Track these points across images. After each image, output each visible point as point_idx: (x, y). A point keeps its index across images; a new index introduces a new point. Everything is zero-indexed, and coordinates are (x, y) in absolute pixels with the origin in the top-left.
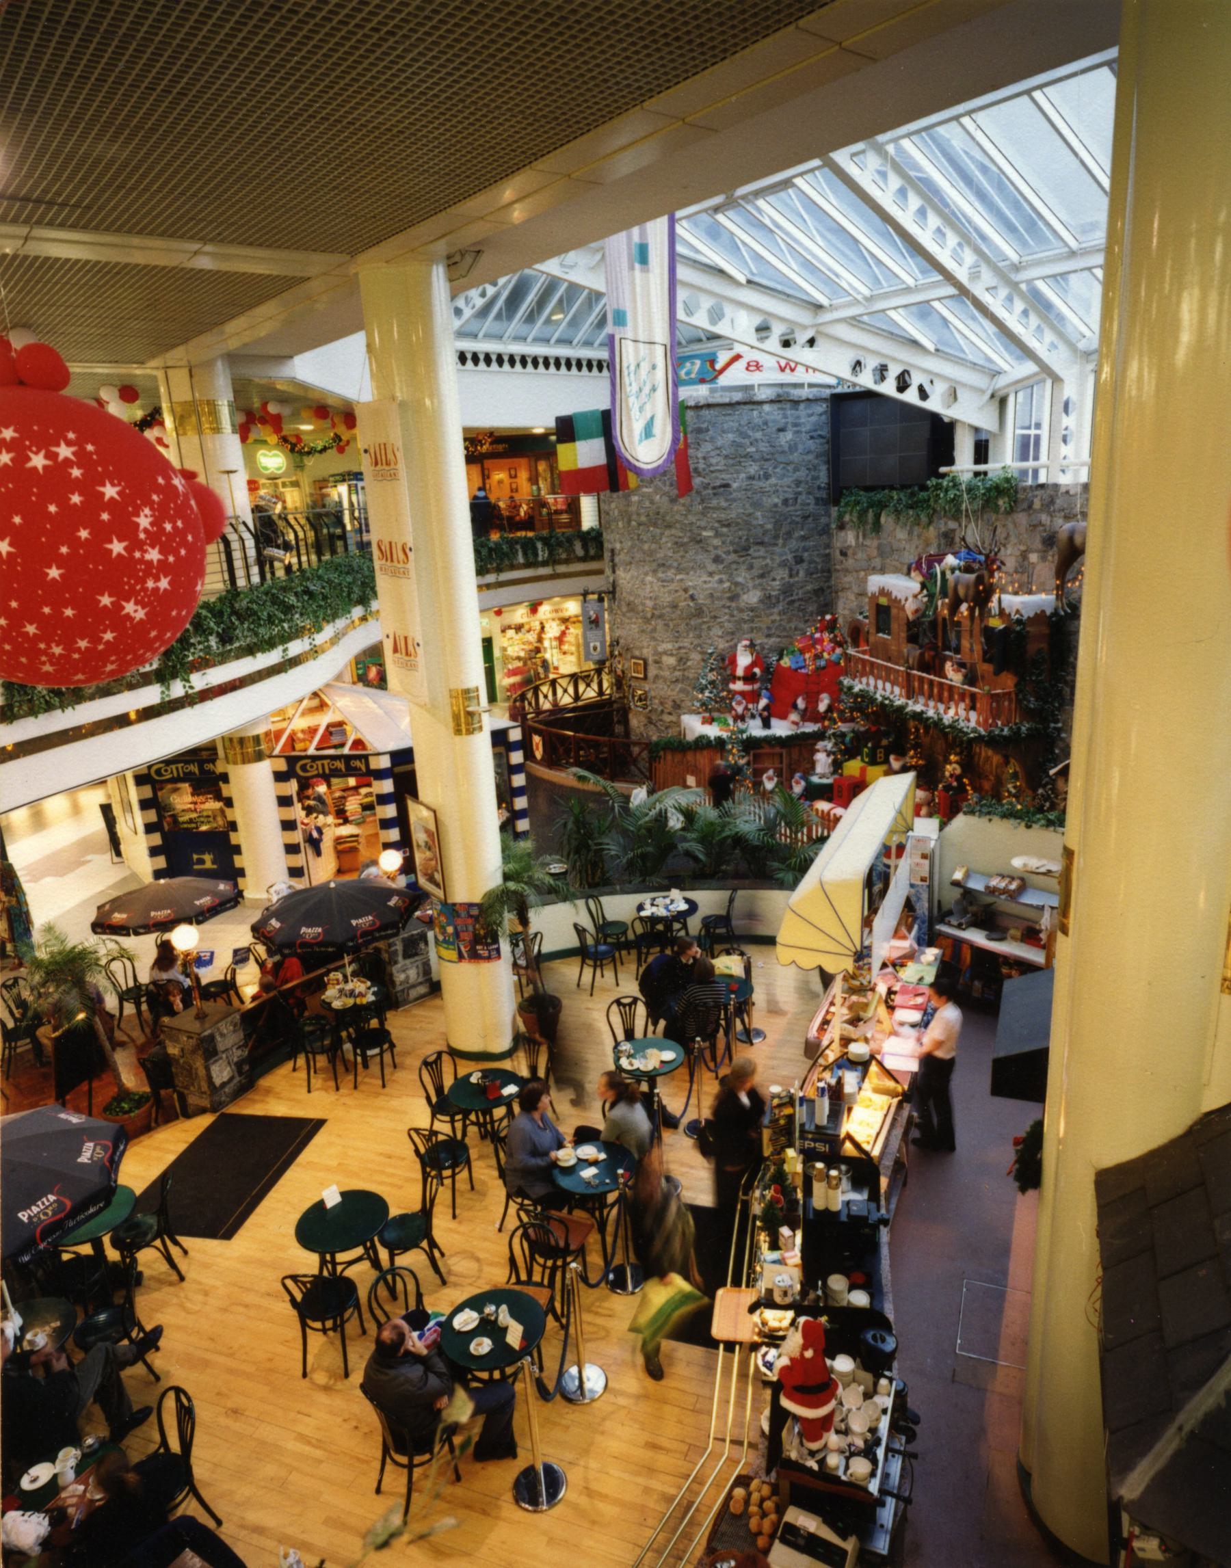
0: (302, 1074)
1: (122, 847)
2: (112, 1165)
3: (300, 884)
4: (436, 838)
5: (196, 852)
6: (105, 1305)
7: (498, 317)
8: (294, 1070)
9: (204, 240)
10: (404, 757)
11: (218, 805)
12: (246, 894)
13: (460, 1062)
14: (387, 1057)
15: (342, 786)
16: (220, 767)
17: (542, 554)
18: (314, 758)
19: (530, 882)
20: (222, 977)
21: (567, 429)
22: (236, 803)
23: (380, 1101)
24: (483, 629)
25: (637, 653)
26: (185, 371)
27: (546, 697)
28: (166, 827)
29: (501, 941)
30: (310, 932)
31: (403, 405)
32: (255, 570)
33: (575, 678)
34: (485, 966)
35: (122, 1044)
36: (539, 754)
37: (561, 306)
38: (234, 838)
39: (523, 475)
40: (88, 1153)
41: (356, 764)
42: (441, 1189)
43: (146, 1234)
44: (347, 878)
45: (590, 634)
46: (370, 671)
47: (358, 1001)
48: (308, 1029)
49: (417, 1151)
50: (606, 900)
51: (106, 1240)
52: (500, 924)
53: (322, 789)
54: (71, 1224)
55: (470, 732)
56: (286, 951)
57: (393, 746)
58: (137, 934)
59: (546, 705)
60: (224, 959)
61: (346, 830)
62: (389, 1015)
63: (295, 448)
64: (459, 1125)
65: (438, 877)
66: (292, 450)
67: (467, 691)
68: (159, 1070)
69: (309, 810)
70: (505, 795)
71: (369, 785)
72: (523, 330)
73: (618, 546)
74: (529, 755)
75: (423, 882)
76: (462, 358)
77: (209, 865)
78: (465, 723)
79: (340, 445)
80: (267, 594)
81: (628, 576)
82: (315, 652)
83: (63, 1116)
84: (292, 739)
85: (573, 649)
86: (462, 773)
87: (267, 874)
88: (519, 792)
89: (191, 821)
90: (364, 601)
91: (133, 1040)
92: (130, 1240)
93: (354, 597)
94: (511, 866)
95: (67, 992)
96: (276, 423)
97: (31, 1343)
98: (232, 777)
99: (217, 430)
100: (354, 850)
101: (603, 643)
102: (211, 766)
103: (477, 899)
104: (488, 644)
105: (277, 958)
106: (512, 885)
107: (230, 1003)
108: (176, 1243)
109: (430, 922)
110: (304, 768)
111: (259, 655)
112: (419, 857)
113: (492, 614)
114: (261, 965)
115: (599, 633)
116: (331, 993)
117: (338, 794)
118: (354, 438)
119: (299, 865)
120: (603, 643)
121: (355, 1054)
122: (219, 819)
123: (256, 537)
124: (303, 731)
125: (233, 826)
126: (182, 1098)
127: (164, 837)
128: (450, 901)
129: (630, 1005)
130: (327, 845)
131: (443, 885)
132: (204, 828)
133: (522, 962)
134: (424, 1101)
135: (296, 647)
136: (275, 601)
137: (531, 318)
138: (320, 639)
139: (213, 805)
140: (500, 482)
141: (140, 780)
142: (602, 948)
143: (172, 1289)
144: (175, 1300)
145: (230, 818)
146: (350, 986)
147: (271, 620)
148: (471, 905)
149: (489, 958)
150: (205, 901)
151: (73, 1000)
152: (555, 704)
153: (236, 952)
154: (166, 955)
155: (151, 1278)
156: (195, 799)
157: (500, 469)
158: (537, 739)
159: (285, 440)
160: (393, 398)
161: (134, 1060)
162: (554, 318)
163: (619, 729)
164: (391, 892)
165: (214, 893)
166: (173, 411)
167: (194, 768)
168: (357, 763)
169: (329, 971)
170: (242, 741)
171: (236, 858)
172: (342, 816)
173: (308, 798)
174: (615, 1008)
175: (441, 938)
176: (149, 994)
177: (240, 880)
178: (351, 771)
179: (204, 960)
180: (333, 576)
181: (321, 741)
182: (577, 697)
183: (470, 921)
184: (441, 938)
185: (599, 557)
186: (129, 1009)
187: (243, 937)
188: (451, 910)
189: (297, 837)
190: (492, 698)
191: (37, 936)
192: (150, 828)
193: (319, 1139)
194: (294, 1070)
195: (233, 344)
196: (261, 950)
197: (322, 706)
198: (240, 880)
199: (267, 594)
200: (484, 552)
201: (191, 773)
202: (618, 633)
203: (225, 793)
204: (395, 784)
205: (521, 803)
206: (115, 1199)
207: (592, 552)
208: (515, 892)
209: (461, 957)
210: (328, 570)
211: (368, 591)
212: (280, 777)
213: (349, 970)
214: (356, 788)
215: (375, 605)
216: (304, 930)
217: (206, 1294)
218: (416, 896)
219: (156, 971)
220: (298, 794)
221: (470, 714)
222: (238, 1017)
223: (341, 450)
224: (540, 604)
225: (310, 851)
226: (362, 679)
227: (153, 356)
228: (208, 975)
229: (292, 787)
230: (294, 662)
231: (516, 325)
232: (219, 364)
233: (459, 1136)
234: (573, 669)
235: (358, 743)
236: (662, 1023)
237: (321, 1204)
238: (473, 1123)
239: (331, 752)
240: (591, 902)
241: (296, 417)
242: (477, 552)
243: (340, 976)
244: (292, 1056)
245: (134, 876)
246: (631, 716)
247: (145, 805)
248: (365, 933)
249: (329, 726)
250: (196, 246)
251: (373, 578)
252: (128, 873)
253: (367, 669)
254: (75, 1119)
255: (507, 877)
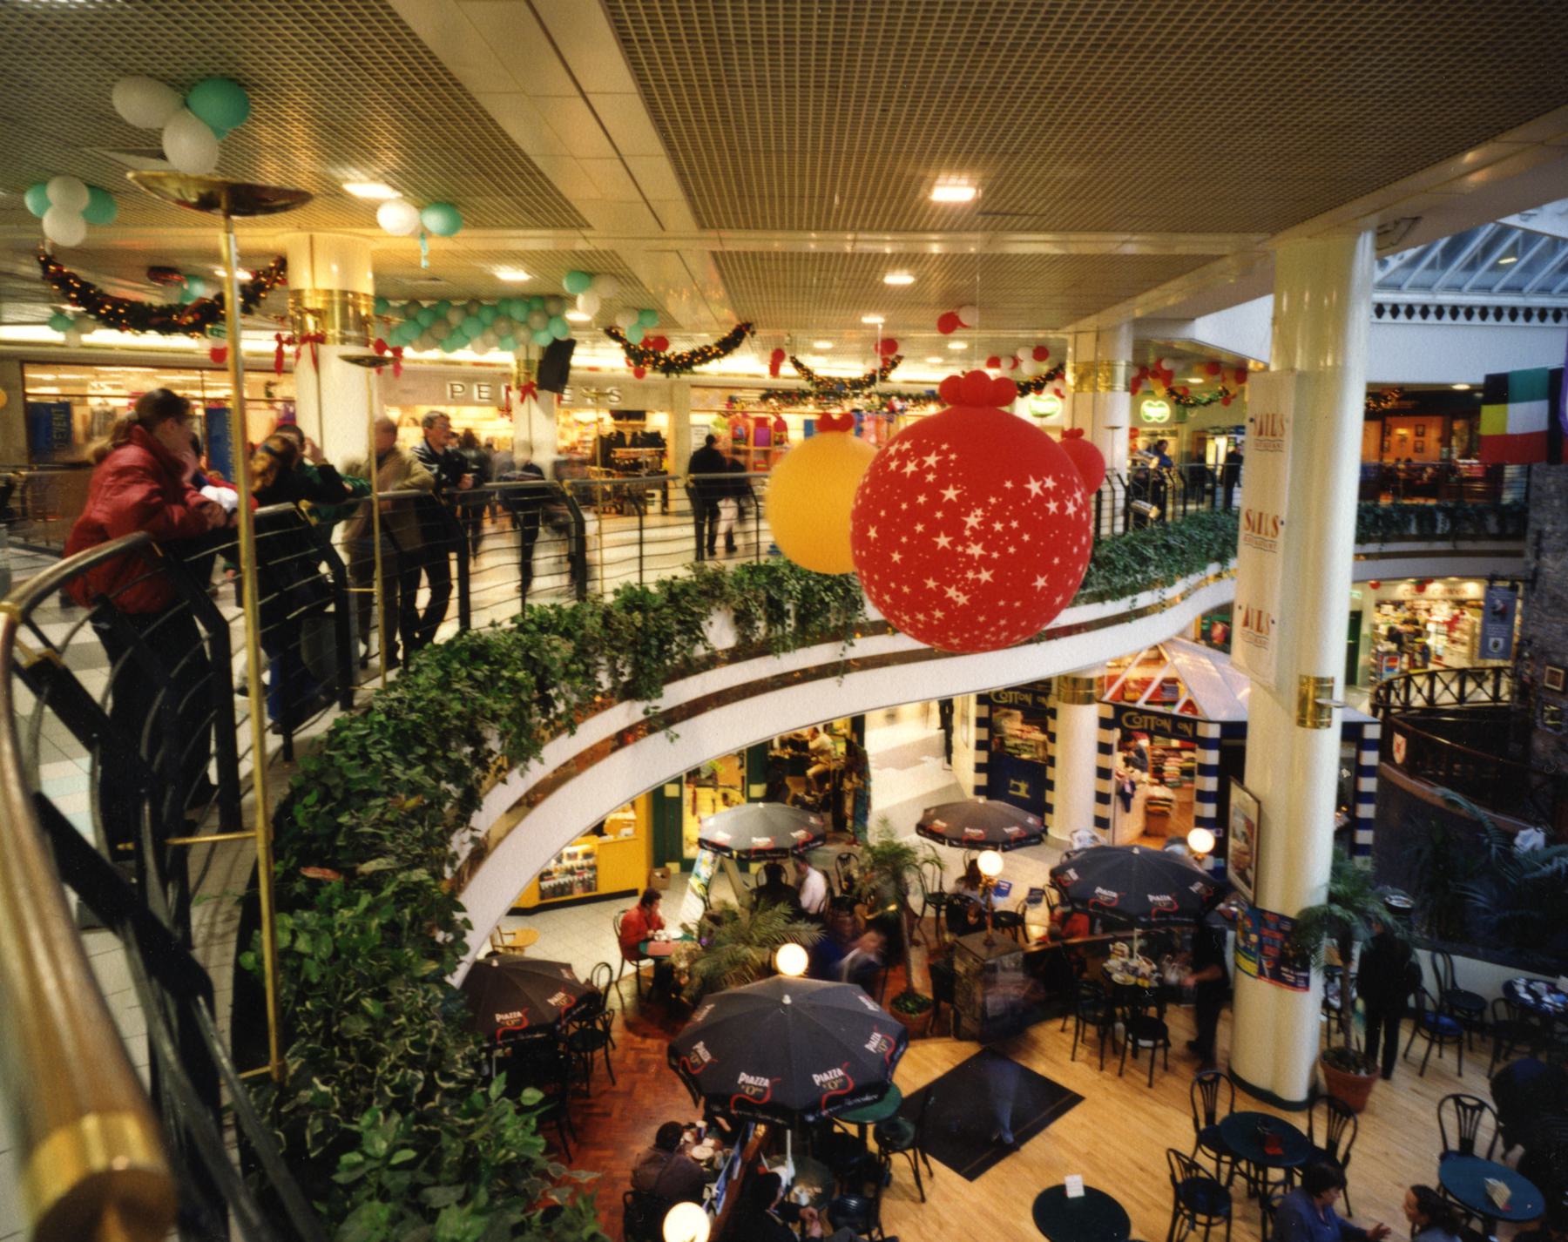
0: (1070, 1038)
1: (954, 756)
2: (891, 1062)
3: (1104, 839)
4: (1256, 831)
5: (1015, 780)
6: (857, 1193)
7: (1432, 266)
8: (1063, 1030)
9: (1134, 232)
10: (1235, 732)
11: (1042, 737)
12: (1050, 831)
13: (1240, 1093)
14: (1160, 1054)
15: (1164, 745)
16: (1051, 702)
17: (1442, 525)
18: (1142, 712)
19: (1361, 913)
20: (1013, 910)
21: (1498, 388)
22: (1058, 739)
23: (1144, 1101)
24: (1353, 601)
25: (1557, 659)
26: (1092, 336)
27: (1419, 691)
28: (994, 747)
29: (1313, 971)
30: (1105, 894)
31: (1302, 376)
32: (1120, 520)
33: (1462, 675)
34: (1289, 993)
35: (917, 944)
36: (1399, 756)
37: (1512, 251)
38: (1051, 773)
39: (1433, 434)
40: (875, 1043)
41: (1184, 728)
42: (1192, 1233)
43: (902, 1139)
44: (1153, 845)
45: (1492, 627)
46: (1215, 631)
47: (1140, 982)
48: (1084, 992)
49: (1173, 1177)
50: (1458, 960)
51: (870, 1129)
52: (1314, 951)
53: (1144, 743)
54: (850, 1103)
55: (1317, 726)
56: (1078, 907)
57: (1224, 716)
58: (951, 845)
59: (1418, 701)
60: (1019, 893)
61: (1160, 792)
62: (1170, 1008)
63: (1181, 399)
64: (1225, 1168)
65: (1250, 874)
66: (1177, 402)
67: (1320, 681)
68: (942, 977)
69: (1128, 761)
70: (1348, 797)
71: (1193, 750)
72: (1460, 278)
73: (1548, 528)
74: (1386, 755)
75: (1232, 874)
76: (1380, 310)
77: (1022, 793)
78: (1311, 712)
79: (1226, 398)
80: (1126, 544)
81: (1558, 566)
82: (1162, 606)
83: (862, 999)
84: (1123, 688)
85: (1466, 638)
86: (1300, 769)
87: (1074, 819)
88: (1367, 798)
89: (1016, 747)
90: (1222, 558)
91: (927, 943)
92: (891, 1140)
93: (1213, 554)
94: (1340, 887)
95: (886, 883)
96: (1167, 377)
97: (797, 1196)
98: (1060, 715)
99: (1111, 388)
100: (1164, 815)
101: (1508, 641)
102: (1043, 700)
103: (1292, 913)
104: (1356, 618)
105: (1068, 909)
106: (1337, 909)
107: (1015, 939)
108: (925, 1161)
109: (1232, 921)
110: (1129, 720)
111: (1109, 603)
112: (1233, 844)
113: (1367, 586)
114: (1052, 908)
115: (1505, 627)
116: (1113, 963)
117: (1158, 752)
118: (1242, 391)
119: (1106, 815)
120: (1508, 641)
121: (1127, 1039)
122: (1041, 750)
123: (1127, 489)
124: (1136, 682)
125: (1051, 761)
126: (957, 1017)
127: (990, 757)
128: (1259, 906)
129: (1473, 1109)
130: (1138, 802)
131: (1256, 885)
132: (1025, 756)
133: (1336, 1003)
134: (1190, 1122)
135: (1144, 599)
136: (1134, 552)
137: (1472, 266)
138: (1171, 593)
139: (1038, 736)
140: (1403, 439)
141: (983, 699)
142: (1446, 1020)
143: (912, 1205)
144: (913, 1219)
145: (1050, 753)
146: (1134, 963)
147: (1126, 570)
148: (1282, 918)
149: (1294, 985)
150: (1013, 830)
151: (889, 890)
152: (1431, 700)
153: (1032, 890)
154: (972, 874)
155: (899, 1185)
156: (1026, 728)
157: (1402, 427)
158: (1399, 740)
159: (1171, 392)
160: (1292, 370)
161: (925, 964)
162: (1504, 262)
163: (1514, 748)
164: (1194, 876)
165: (1024, 825)
166: (1075, 370)
167: (1028, 698)
168: (1185, 727)
169: (1113, 941)
170: (1075, 681)
171: (1048, 793)
172: (1159, 775)
173: (1128, 749)
174: (1451, 1103)
175: (1242, 944)
176: (949, 903)
177: (1047, 816)
178: (1176, 733)
179: (1002, 891)
180: (1196, 533)
181: (1154, 694)
182: (1461, 698)
183: (1278, 936)
184: (1242, 944)
185: (1519, 536)
186: (930, 912)
187: (1041, 879)
188: (1259, 916)
189: (1110, 787)
190: (1351, 679)
191: (873, 822)
192: (980, 745)
193: (1072, 1117)
194: (1063, 1030)
195: (1138, 313)
196: (1054, 895)
197: (1158, 659)
198: (1047, 816)
199: (1126, 544)
200: (1369, 518)
201: (1025, 703)
202: (1531, 631)
203: (1050, 729)
204: (1222, 757)
205: (1366, 811)
206: (889, 1096)
207: (1510, 530)
208: (1340, 919)
209: (1261, 973)
210: (1189, 515)
211: (1229, 550)
212: (1105, 724)
213: (1137, 944)
214: (1178, 751)
215: (1233, 563)
216: (1099, 890)
217: (941, 1226)
218: (1219, 884)
219: (962, 886)
220: (1120, 743)
221: (1320, 708)
222: (1021, 955)
223: (1226, 402)
224: (1430, 580)
225: (1119, 805)
226: (1205, 636)
227: (1068, 323)
228: (1002, 904)
229: (1115, 735)
230: (1140, 613)
231: (1452, 273)
232: (1124, 329)
233: (1223, 1181)
234: (1465, 664)
235: (1189, 705)
236: (1519, 1150)
237: (1061, 1189)
238: (1242, 1174)
239: (1160, 709)
240: (1439, 958)
241: (1189, 371)
242: (1361, 518)
243: (1126, 949)
244: (1063, 1015)
245: (957, 787)
246: (1534, 736)
247: (980, 723)
248: (1161, 913)
249: (1166, 680)
250: (1127, 237)
251: (1235, 537)
252: (952, 781)
253: (1213, 625)
254: (871, 1006)
255: (1333, 898)
